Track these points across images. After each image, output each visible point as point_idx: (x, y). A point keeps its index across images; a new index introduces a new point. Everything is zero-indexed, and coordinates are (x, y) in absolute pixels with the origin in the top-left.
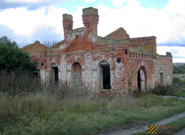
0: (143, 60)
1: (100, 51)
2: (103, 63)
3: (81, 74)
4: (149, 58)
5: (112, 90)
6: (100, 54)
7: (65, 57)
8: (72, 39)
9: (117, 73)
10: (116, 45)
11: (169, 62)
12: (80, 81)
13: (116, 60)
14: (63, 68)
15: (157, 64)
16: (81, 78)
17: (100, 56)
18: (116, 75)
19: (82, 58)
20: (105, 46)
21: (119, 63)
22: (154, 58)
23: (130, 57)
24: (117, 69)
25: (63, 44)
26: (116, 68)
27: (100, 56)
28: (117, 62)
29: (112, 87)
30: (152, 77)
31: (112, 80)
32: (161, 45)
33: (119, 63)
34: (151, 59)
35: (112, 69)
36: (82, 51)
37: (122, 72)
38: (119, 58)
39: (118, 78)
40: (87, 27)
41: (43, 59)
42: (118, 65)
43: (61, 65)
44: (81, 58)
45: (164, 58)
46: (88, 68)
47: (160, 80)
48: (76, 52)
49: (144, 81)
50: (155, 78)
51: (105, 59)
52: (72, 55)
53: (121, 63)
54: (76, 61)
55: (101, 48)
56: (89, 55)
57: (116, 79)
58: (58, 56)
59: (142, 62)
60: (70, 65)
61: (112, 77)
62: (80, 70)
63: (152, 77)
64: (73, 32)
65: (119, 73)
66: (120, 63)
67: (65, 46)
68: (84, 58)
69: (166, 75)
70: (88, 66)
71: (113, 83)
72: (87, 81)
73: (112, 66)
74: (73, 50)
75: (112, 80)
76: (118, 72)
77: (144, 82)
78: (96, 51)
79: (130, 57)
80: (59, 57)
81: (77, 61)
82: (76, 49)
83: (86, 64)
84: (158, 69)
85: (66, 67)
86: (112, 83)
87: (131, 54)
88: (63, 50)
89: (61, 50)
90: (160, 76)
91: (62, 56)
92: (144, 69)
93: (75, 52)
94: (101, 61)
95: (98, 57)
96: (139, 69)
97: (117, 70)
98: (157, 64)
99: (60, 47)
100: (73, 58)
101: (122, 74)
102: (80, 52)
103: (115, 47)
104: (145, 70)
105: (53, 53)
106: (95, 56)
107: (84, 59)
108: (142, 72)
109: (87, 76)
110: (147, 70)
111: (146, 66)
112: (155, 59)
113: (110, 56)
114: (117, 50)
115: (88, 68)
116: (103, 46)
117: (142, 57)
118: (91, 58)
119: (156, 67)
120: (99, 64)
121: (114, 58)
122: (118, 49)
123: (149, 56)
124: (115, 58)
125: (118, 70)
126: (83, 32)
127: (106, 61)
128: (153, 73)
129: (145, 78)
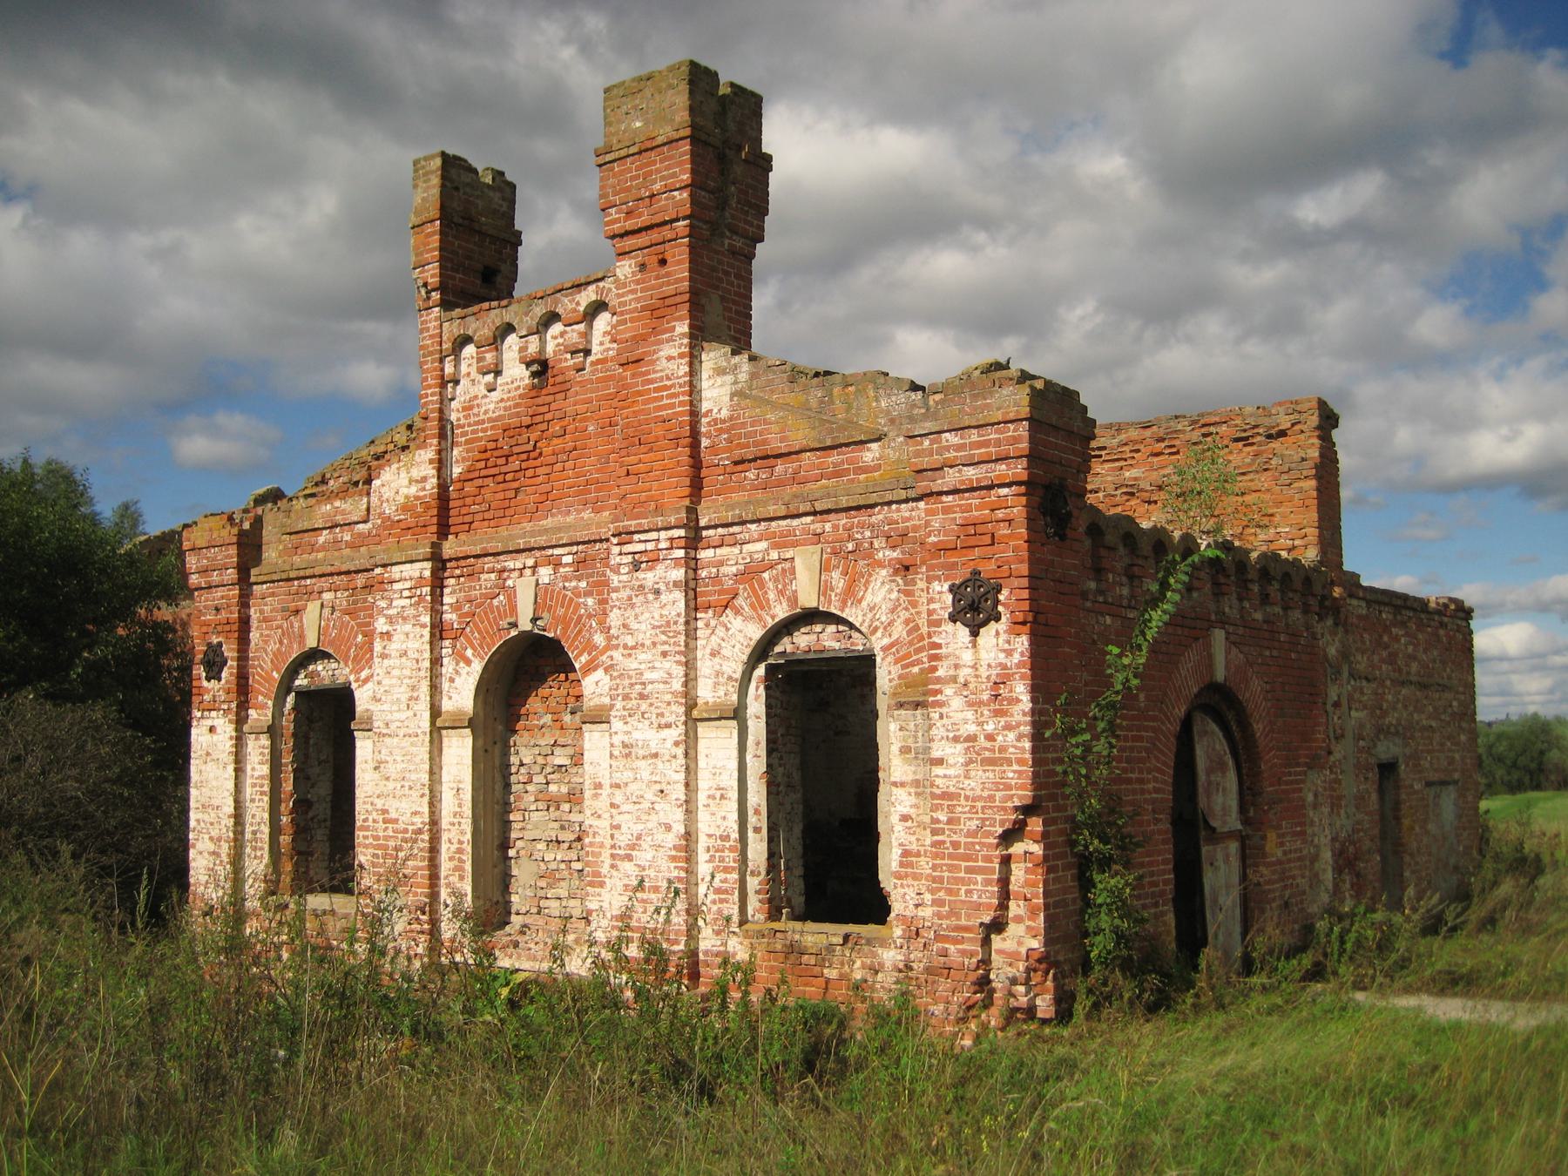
0: (1223, 622)
1: (772, 510)
2: (802, 641)
3: (578, 759)
4: (1278, 610)
5: (898, 932)
6: (776, 546)
8: (495, 395)
9: (956, 739)
11: (1444, 663)
12: (568, 836)
13: (949, 598)
14: (402, 693)
15: (1345, 669)
16: (574, 797)
18: (940, 762)
19: (588, 594)
21: (975, 634)
22: (1321, 619)
23: (1098, 571)
24: (957, 703)
25: (404, 448)
26: (949, 691)
28: (953, 619)
29: (902, 896)
30: (1310, 798)
31: (895, 819)
33: (975, 634)
34: (1296, 615)
35: (901, 705)
36: (595, 521)
37: (1011, 736)
38: (975, 577)
39: (962, 807)
40: (643, 267)
42: (967, 657)
43: (379, 667)
44: (577, 593)
45: (1403, 624)
46: (642, 697)
47: (1376, 831)
48: (528, 526)
49: (1231, 835)
50: (1335, 804)
51: (824, 589)
52: (489, 562)
53: (1002, 625)
54: (525, 625)
55: (781, 484)
56: (654, 561)
57: (943, 817)
58: (360, 580)
59: (1219, 635)
60: (468, 662)
61: (900, 793)
62: (567, 718)
63: (1310, 798)
65: (982, 742)
66: (991, 635)
68: (601, 587)
69: (1429, 784)
70: (648, 676)
71: (906, 853)
73: (896, 670)
74: (503, 513)
75: (905, 818)
76: (972, 728)
77: (1234, 847)
78: (730, 516)
79: (1098, 571)
80: (368, 587)
81: (534, 620)
82: (528, 498)
83: (630, 650)
84: (1362, 726)
86: (896, 853)
87: (1110, 538)
88: (405, 508)
89: (388, 510)
90: (1374, 796)
91: (396, 571)
92: (1230, 716)
93: (522, 532)
94: (781, 612)
95: (751, 573)
96: (1181, 711)
97: (956, 712)
98: (1345, 669)
99: (376, 483)
102: (568, 527)
104: (1244, 724)
105: (313, 548)
106: (721, 563)
107: (603, 602)
108: (1210, 744)
109: (627, 775)
110: (1258, 728)
111: (1256, 685)
112: (1330, 622)
113: (881, 564)
115: (642, 697)
117: (1218, 594)
119: (1337, 705)
120: (761, 651)
121: (921, 584)
122: (971, 473)
123: (1274, 589)
124: (929, 580)
125: (970, 704)
126: (603, 322)
127: (839, 620)
128: (1315, 763)
129: (1243, 808)
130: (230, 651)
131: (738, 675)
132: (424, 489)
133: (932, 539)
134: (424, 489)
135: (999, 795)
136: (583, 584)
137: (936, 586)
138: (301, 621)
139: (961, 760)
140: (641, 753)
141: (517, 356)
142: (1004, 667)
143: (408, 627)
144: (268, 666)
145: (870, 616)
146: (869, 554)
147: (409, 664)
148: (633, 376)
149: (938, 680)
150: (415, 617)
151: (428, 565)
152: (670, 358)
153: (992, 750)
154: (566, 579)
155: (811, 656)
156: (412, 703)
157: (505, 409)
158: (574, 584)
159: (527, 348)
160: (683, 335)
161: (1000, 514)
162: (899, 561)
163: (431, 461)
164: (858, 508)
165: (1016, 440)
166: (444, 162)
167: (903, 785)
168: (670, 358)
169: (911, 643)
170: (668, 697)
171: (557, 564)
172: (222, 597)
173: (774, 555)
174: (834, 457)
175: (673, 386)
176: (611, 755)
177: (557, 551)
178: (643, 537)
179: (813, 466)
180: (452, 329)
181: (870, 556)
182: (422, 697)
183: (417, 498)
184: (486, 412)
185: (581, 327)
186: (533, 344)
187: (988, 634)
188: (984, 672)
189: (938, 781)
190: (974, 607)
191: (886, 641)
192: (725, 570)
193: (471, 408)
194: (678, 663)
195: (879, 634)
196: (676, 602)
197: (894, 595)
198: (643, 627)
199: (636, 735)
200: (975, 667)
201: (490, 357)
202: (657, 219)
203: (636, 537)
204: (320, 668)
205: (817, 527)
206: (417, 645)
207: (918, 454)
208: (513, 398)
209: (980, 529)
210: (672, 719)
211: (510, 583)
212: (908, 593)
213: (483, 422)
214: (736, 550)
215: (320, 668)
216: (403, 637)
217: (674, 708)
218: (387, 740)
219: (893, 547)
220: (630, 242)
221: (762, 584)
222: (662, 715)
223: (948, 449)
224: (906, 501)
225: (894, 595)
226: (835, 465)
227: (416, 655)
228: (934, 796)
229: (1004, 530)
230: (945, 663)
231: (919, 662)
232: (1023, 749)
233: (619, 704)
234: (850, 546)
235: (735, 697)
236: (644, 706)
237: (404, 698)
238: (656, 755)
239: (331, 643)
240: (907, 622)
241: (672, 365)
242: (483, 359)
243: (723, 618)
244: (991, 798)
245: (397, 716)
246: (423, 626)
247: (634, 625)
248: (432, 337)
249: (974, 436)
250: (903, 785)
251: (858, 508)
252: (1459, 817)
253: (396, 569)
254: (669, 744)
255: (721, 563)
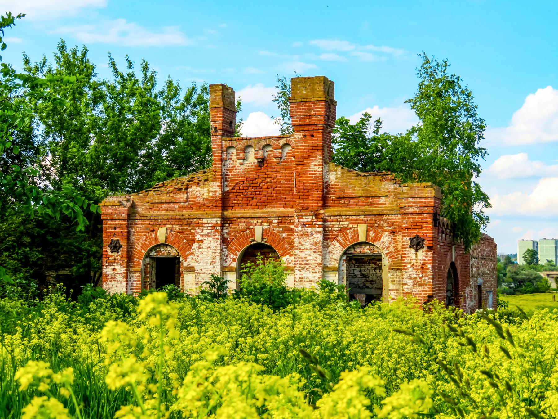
6: (352, 223)
7: (216, 224)
8: (243, 167)
9: (410, 279)
10: (411, 200)
13: (121, 244)
17: (350, 229)
18: (405, 284)
19: (283, 232)
20: (368, 197)
21: (417, 251)
26: (408, 266)
27: (350, 229)
28: (410, 247)
32: (320, 101)
33: (417, 251)
37: (427, 278)
38: (417, 237)
40: (305, 136)
41: (115, 228)
53: (424, 250)
64: (250, 146)
65: (418, 279)
67: (218, 189)
72: (478, 372)
76: (415, 276)
85: (218, 259)
91: (205, 221)
95: (343, 230)
100: (249, 228)
101: (426, 282)
103: (407, 205)
113: (386, 231)
114: (412, 214)
115: (306, 264)
116: (361, 199)
118: (319, 232)
122: (416, 209)
124: (403, 236)
125: (414, 269)
126: (287, 150)
130: (123, 242)
131: (338, 259)
132: (215, 195)
133: (404, 226)
134: (215, 195)
135: (423, 293)
136: (281, 229)
137: (405, 238)
138: (156, 234)
139: (412, 284)
140: (306, 280)
141: (253, 156)
142: (424, 260)
143: (211, 239)
144: (139, 248)
145: (382, 244)
146: (382, 228)
147: (211, 251)
148: (301, 169)
149: (406, 263)
150: (214, 236)
151: (220, 219)
152: (315, 165)
153: (421, 282)
154: (274, 227)
155: (361, 254)
156: (212, 263)
157: (247, 172)
158: (277, 229)
159: (257, 154)
160: (320, 159)
161: (424, 221)
162: (392, 230)
163: (218, 186)
164: (379, 215)
165: (430, 202)
166: (223, 89)
167: (392, 290)
168: (315, 165)
169: (395, 252)
170: (316, 265)
171: (271, 223)
172: (118, 224)
173: (351, 226)
174: (370, 200)
175: (316, 174)
176: (295, 281)
177: (273, 219)
178: (307, 217)
179: (363, 202)
180: (225, 144)
181: (383, 228)
182: (217, 261)
183: (212, 197)
184: (239, 172)
185: (280, 150)
186: (260, 154)
187: (420, 252)
188: (419, 261)
189: (405, 289)
190: (418, 244)
191: (387, 252)
192: (333, 229)
193: (233, 170)
194: (320, 255)
195: (385, 250)
196: (320, 237)
197: (390, 239)
198: (307, 244)
199: (304, 275)
200: (416, 260)
201: (241, 155)
202: (311, 123)
203: (304, 217)
204: (162, 250)
205: (365, 219)
206: (215, 244)
207: (401, 203)
208: (251, 169)
209: (418, 224)
210: (317, 271)
211: (251, 227)
212: (394, 239)
213: (238, 175)
214: (338, 223)
215: (162, 250)
216: (208, 242)
217: (318, 268)
218: (201, 274)
219: (390, 226)
220: (298, 128)
221: (347, 234)
222: (314, 269)
223: (410, 202)
224: (395, 214)
225: (390, 239)
226: (370, 202)
227: (214, 248)
228: (403, 293)
229: (425, 225)
230: (407, 258)
231: (397, 258)
232: (430, 282)
233: (298, 266)
234: (376, 225)
235: (337, 265)
236: (307, 267)
237: (209, 262)
238: (311, 281)
239: (171, 242)
240: (394, 247)
241: (316, 168)
242: (239, 155)
243: (333, 242)
244: (421, 294)
245: (205, 267)
246: (218, 239)
247: (303, 243)
248: (218, 145)
249: (418, 200)
250: (392, 290)
251: (379, 215)
252: (493, 303)
253: (204, 220)
254: (316, 278)
255: (333, 227)
